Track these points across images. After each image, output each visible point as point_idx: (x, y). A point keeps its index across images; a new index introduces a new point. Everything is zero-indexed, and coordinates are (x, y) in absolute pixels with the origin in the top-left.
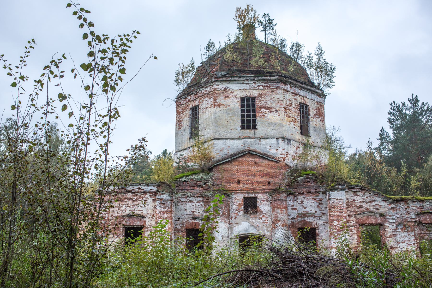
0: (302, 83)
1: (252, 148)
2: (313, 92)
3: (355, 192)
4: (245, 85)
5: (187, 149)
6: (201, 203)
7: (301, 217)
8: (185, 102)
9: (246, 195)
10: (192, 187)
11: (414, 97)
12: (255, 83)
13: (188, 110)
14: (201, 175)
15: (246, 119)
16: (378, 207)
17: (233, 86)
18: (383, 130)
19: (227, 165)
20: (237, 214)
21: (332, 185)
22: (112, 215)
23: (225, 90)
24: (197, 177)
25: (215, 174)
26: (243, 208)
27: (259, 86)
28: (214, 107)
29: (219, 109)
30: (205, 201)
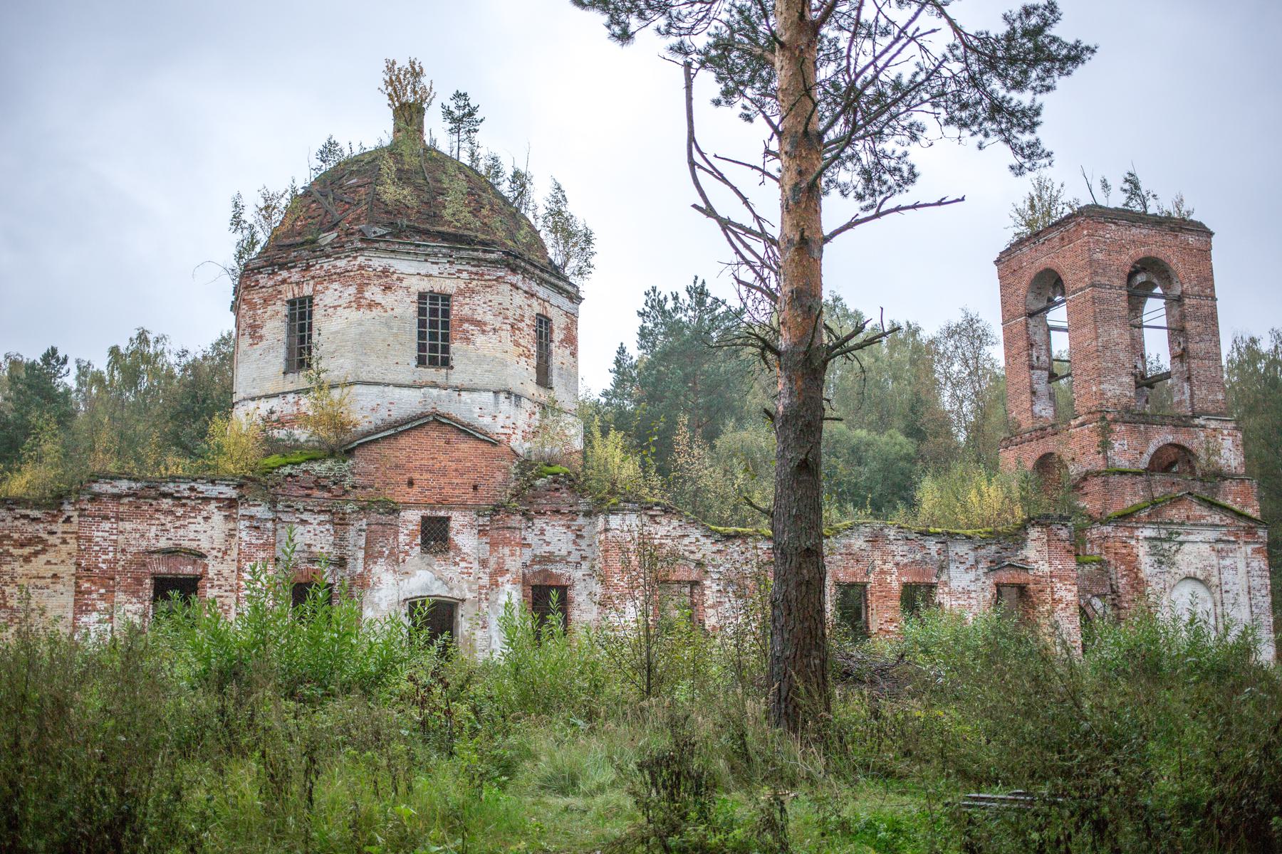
0: (542, 271)
1: (441, 410)
2: (561, 291)
3: (652, 517)
4: (429, 264)
5: (275, 396)
6: (327, 526)
7: (540, 562)
8: (271, 283)
9: (428, 513)
10: (307, 488)
11: (699, 283)
12: (451, 263)
13: (279, 303)
14: (329, 463)
15: (428, 342)
16: (693, 548)
17: (402, 266)
18: (622, 351)
19: (385, 444)
20: (407, 553)
21: (614, 501)
22: (123, 550)
23: (385, 272)
24: (319, 468)
25: (359, 462)
26: (419, 541)
27: (460, 271)
28: (358, 308)
29: (369, 315)
30: (336, 521)
